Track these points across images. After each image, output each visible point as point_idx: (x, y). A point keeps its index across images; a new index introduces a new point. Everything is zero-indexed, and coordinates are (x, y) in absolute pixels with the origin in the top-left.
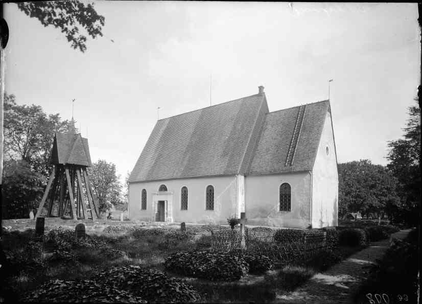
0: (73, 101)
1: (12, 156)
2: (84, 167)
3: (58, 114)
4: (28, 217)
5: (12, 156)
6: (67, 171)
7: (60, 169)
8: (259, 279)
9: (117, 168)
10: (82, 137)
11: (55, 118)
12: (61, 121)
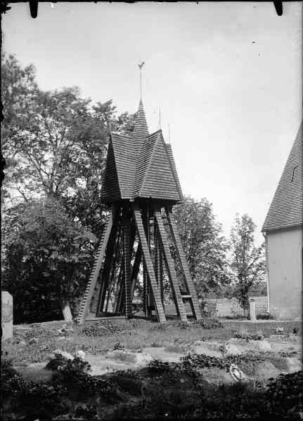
0: (140, 67)
1: (83, 346)
2: (168, 204)
3: (109, 103)
4: (61, 317)
5: (83, 346)
6: (138, 215)
7: (123, 210)
8: (209, 347)
9: (215, 211)
10: (166, 143)
11: (105, 109)
12: (116, 115)
